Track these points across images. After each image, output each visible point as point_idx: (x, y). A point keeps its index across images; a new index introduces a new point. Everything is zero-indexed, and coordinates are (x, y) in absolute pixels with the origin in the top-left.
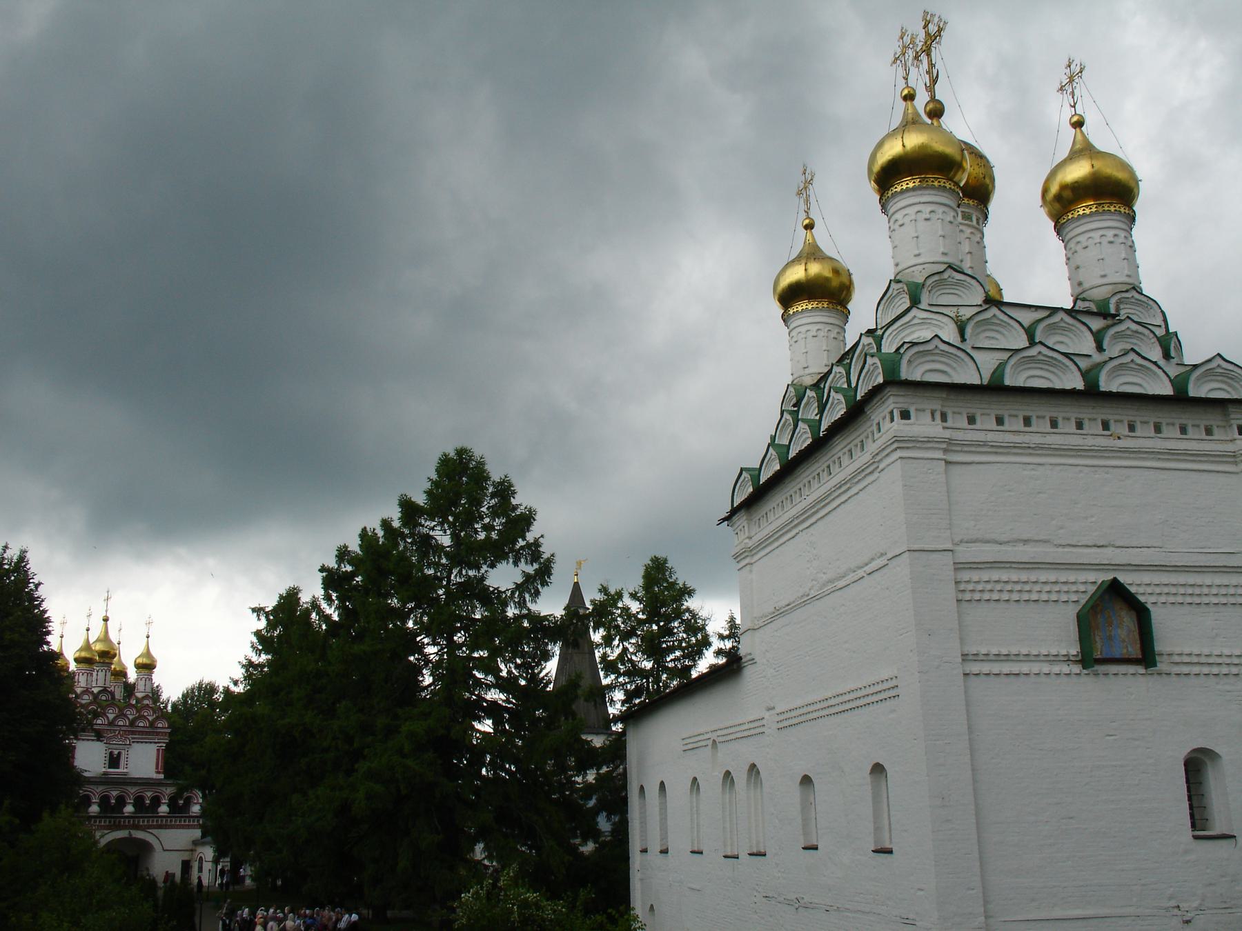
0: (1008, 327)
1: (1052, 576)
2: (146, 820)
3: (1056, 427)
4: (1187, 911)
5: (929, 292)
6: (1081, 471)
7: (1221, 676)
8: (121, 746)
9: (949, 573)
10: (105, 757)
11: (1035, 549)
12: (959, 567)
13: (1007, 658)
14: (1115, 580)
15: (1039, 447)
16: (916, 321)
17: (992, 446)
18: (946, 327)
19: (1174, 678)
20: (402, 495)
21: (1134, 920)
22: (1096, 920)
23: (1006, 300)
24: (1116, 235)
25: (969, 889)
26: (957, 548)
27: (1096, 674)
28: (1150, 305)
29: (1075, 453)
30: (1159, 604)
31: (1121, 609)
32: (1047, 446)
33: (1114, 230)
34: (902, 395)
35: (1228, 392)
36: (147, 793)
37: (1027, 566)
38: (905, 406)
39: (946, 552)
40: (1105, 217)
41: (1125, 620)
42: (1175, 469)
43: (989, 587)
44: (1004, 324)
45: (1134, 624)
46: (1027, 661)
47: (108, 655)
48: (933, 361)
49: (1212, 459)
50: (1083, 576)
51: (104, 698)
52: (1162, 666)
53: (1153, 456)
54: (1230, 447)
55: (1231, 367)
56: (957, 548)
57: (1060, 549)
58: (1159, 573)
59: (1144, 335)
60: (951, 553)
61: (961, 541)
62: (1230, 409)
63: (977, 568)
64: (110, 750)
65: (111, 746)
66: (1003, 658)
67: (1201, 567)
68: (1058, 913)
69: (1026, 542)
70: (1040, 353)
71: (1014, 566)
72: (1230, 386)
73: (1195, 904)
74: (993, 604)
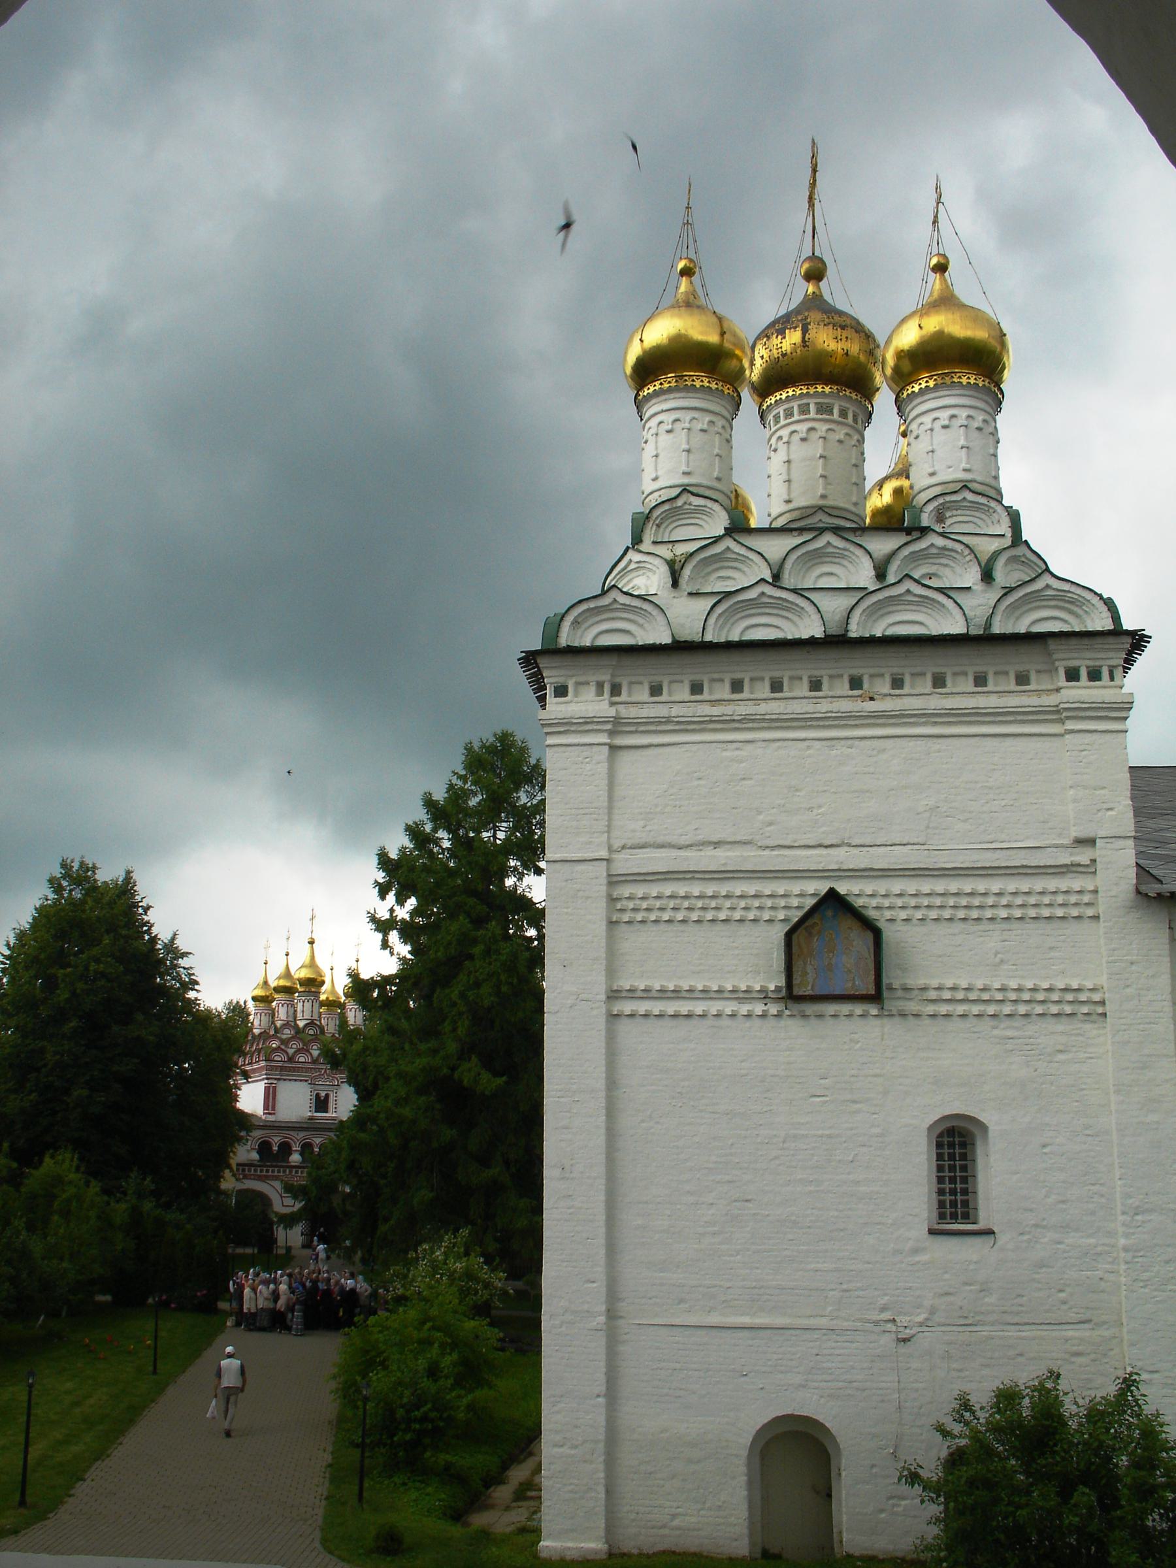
0: (748, 561)
1: (751, 888)
2: (288, 1170)
3: (781, 691)
4: (906, 1327)
5: (658, 526)
6: (809, 748)
7: (740, 1018)
8: (327, 1087)
10: (311, 1100)
11: (729, 854)
12: (613, 881)
13: (677, 995)
14: (832, 894)
15: (745, 719)
16: (632, 566)
17: (679, 723)
18: (657, 571)
20: (425, 794)
21: (825, 1335)
22: (769, 1331)
23: (753, 524)
26: (614, 856)
27: (805, 1016)
28: (992, 508)
29: (804, 724)
31: (849, 928)
32: (758, 717)
33: (950, 409)
35: (1065, 621)
36: (273, 1138)
37: (716, 876)
38: (561, 680)
41: (854, 943)
45: (869, 949)
46: (706, 998)
47: (313, 984)
48: (613, 619)
49: (1019, 718)
50: (796, 887)
51: (311, 1032)
52: (891, 1005)
53: (924, 720)
54: (1050, 700)
55: (1066, 587)
56: (614, 856)
57: (767, 852)
58: (919, 879)
60: (605, 862)
61: (623, 847)
64: (316, 1092)
65: (316, 1087)
68: (715, 1319)
69: (717, 844)
70: (763, 594)
73: (920, 1318)
74: (663, 926)
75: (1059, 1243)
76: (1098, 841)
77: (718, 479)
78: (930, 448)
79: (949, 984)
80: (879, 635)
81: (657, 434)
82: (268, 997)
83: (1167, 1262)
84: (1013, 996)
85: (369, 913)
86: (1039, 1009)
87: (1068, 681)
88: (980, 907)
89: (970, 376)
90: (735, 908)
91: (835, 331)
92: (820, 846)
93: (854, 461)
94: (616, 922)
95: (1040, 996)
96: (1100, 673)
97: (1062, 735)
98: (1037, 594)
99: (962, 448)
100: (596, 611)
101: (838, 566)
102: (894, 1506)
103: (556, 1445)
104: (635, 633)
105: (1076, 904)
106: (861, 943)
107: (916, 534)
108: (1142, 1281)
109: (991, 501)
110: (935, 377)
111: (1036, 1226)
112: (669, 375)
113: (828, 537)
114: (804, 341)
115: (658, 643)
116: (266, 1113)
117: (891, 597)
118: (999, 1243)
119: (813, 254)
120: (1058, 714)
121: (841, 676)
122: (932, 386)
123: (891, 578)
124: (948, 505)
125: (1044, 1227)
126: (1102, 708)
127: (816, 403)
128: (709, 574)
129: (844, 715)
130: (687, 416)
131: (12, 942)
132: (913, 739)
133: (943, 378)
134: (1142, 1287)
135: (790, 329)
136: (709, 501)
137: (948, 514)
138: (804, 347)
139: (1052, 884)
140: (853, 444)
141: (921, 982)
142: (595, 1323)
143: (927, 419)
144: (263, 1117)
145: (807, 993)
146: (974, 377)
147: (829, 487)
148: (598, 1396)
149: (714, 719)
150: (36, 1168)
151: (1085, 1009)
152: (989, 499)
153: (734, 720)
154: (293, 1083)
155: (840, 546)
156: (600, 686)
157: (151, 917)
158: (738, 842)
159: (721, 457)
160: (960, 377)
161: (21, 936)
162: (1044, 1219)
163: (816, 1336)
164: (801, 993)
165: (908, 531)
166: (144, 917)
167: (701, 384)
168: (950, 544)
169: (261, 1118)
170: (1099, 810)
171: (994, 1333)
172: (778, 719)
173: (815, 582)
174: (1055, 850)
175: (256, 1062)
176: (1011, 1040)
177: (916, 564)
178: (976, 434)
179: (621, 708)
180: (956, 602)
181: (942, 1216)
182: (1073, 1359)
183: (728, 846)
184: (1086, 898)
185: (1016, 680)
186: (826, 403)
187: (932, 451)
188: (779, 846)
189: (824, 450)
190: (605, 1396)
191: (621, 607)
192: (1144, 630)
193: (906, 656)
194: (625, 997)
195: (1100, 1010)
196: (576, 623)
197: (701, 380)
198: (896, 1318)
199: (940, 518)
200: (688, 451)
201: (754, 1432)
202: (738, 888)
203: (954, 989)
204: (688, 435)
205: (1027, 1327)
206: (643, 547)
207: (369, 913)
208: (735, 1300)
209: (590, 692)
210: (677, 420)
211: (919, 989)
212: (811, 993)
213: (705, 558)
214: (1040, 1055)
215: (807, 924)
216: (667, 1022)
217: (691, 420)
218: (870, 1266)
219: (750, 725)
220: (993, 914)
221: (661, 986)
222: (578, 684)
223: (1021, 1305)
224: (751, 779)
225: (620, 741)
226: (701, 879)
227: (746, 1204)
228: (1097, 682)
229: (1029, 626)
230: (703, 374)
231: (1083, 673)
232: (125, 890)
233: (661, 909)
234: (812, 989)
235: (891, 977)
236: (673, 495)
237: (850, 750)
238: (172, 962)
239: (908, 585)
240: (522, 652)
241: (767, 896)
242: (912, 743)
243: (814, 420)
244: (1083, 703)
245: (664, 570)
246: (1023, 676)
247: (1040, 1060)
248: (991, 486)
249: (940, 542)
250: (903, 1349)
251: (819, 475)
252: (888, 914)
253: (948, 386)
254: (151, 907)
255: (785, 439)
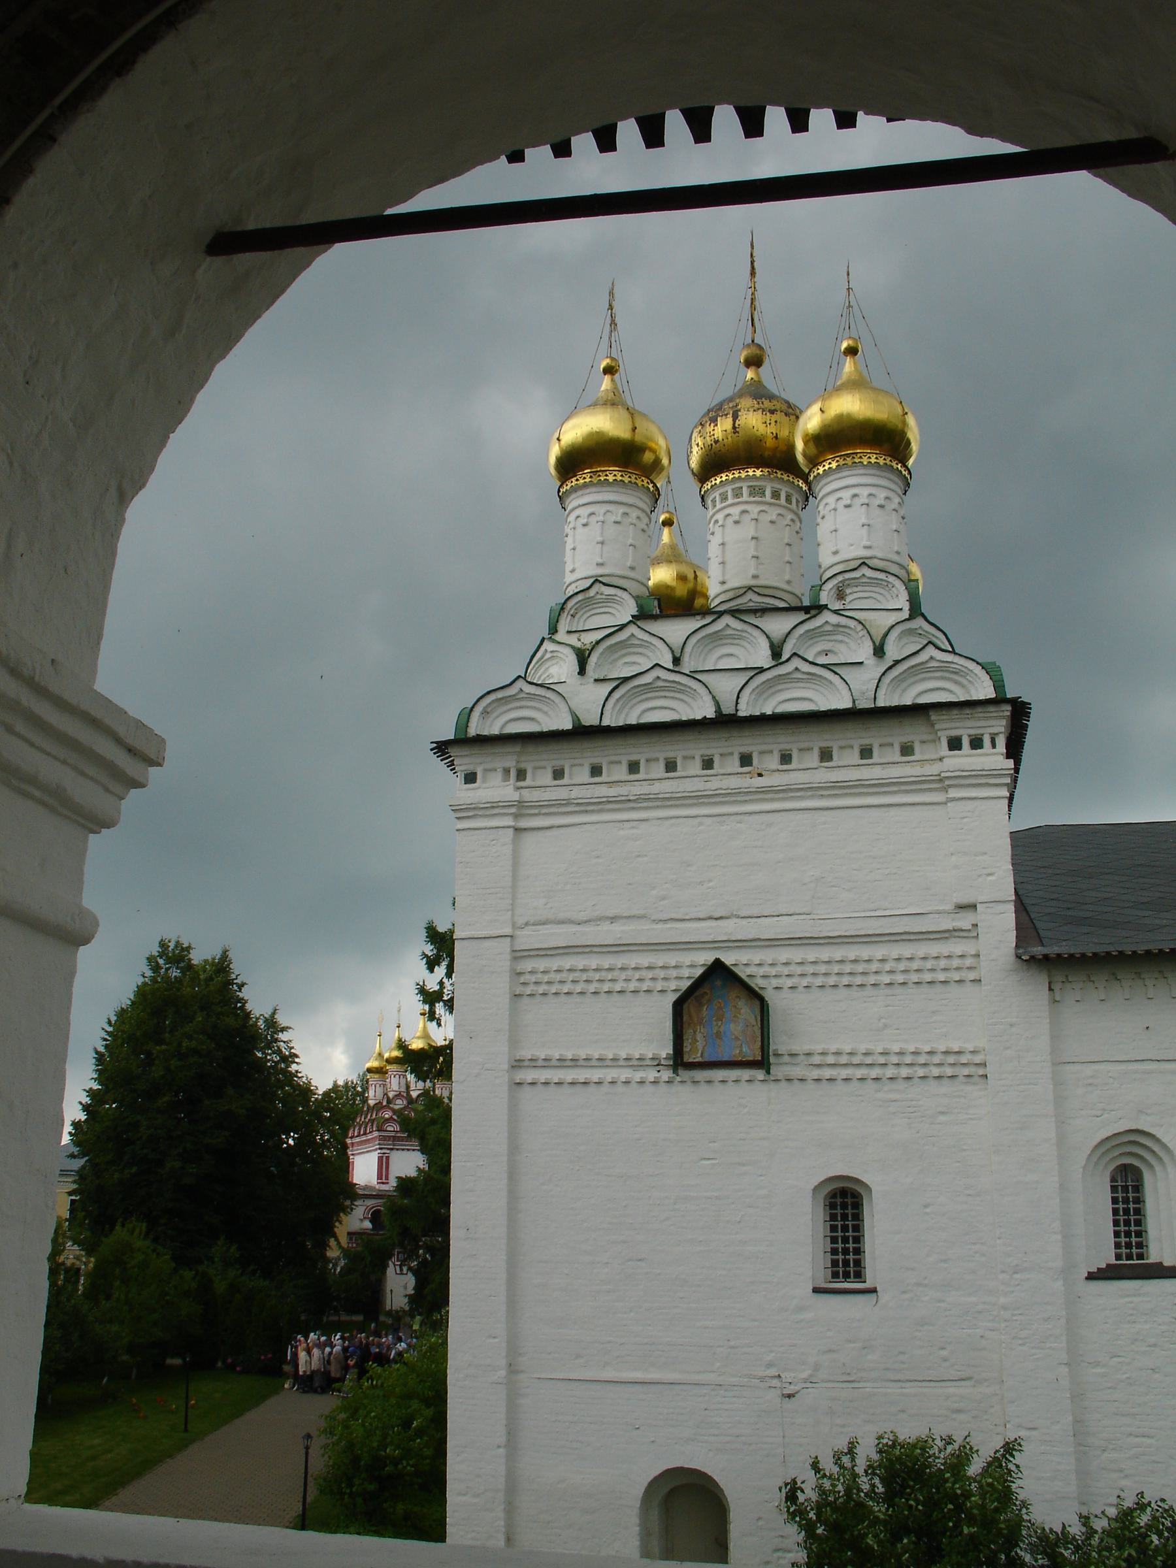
1: (644, 960)
6: (701, 824)
9: (505, 963)
11: (626, 928)
12: (518, 955)
13: (575, 1062)
14: (718, 965)
16: (548, 655)
17: (578, 804)
19: (811, 1086)
21: (713, 1390)
22: (660, 1387)
24: (626, 514)
25: (490, 1337)
26: (518, 933)
28: (891, 583)
29: (695, 801)
30: (801, 989)
31: (738, 997)
34: (467, 755)
35: (951, 691)
38: (470, 768)
39: (503, 939)
40: (844, 474)
41: (742, 1011)
42: (847, 808)
43: (558, 977)
44: (647, 645)
48: (521, 707)
49: (903, 788)
50: (687, 958)
54: (934, 769)
56: (518, 933)
57: (660, 926)
59: (849, 628)
60: (509, 938)
61: (527, 924)
62: (933, 718)
63: (546, 955)
66: (568, 1063)
67: (852, 936)
68: (609, 1374)
69: (613, 919)
71: (595, 949)
72: (956, 682)
73: (805, 1375)
74: (563, 998)
75: (940, 1301)
76: (978, 906)
77: (632, 568)
78: (833, 528)
79: (833, 1048)
80: (769, 712)
81: (574, 528)
82: (382, 1068)
83: (1046, 1320)
84: (895, 1060)
85: (418, 985)
86: (921, 1072)
87: (950, 750)
88: (932, 970)
89: (871, 455)
90: (564, 982)
91: (764, 416)
92: (711, 918)
93: (786, 541)
94: (520, 995)
95: (922, 1059)
96: (982, 741)
97: (945, 803)
98: (922, 667)
99: (863, 526)
100: (504, 701)
101: (738, 647)
102: (779, 1558)
103: (460, 1494)
104: (539, 720)
105: (958, 969)
106: (747, 1012)
107: (813, 612)
108: (1020, 1338)
109: (889, 576)
110: (838, 459)
111: (918, 1284)
112: (586, 471)
113: (727, 620)
114: (734, 427)
115: (560, 729)
116: (380, 1183)
117: (780, 675)
118: (882, 1301)
119: (753, 341)
120: (942, 782)
121: (731, 754)
122: (834, 467)
123: (785, 657)
124: (847, 582)
125: (926, 1286)
126: (982, 775)
127: (749, 487)
128: (615, 660)
129: (733, 791)
130: (600, 509)
131: (113, 1019)
132: (800, 812)
133: (844, 459)
134: (1020, 1345)
135: (722, 416)
136: (619, 590)
137: (848, 591)
138: (734, 433)
139: (934, 949)
140: (786, 523)
141: (806, 1048)
142: (496, 1377)
143: (831, 500)
144: (377, 1187)
145: (697, 1060)
146: (875, 456)
147: (761, 567)
148: (499, 1447)
149: (611, 799)
150: (106, 1236)
151: (966, 1071)
152: (887, 574)
153: (629, 800)
154: (405, 1152)
155: (739, 628)
156: (507, 771)
157: (244, 994)
158: (634, 916)
159: (635, 547)
160: (861, 457)
161: (121, 1014)
162: (926, 1278)
163: (705, 1391)
164: (691, 1060)
165: (806, 610)
166: (238, 993)
167: (614, 478)
168: (843, 621)
169: (375, 1188)
170: (979, 876)
171: (875, 1390)
172: (671, 798)
173: (714, 666)
174: (937, 916)
175: (370, 1132)
176: (894, 1103)
177: (811, 642)
178: (878, 511)
179: (525, 792)
180: (842, 678)
181: (835, 1275)
182: (954, 1416)
183: (625, 920)
184: (968, 962)
185: (901, 751)
186: (757, 486)
187: (835, 531)
188: (672, 919)
189: (756, 531)
190: (505, 1446)
191: (526, 696)
192: (1020, 697)
193: (793, 732)
194: (528, 1067)
195: (981, 1071)
196: (485, 713)
197: (613, 474)
198: (781, 1375)
199: (841, 595)
200: (602, 543)
201: (646, 1484)
202: (633, 960)
203: (838, 1053)
204: (602, 528)
205: (909, 1384)
206: (558, 637)
207: (418, 985)
208: (628, 1355)
209: (497, 778)
210: (593, 514)
211: (804, 1054)
212: (700, 1059)
213: (612, 646)
214: (923, 1117)
215: (697, 994)
216: (566, 1089)
217: (605, 514)
218: (756, 1323)
219: (645, 804)
220: (876, 980)
221: (561, 1055)
222: (486, 770)
223: (903, 1363)
224: (646, 856)
225: (523, 823)
226: (599, 952)
227: (639, 1263)
228: (979, 750)
229: (915, 698)
230: (617, 469)
231: (966, 742)
232: (222, 966)
233: (562, 982)
234: (702, 1056)
235: (778, 1043)
236: (588, 585)
237: (739, 825)
238: (272, 1037)
239: (796, 663)
240: (432, 743)
241: (661, 967)
242: (800, 816)
243: (747, 502)
244: (963, 771)
245: (572, 660)
246: (907, 747)
247: (922, 1121)
248: (892, 562)
249: (834, 619)
250: (789, 1404)
251: (751, 555)
252: (775, 982)
253: (850, 467)
254: (245, 984)
255: (720, 523)
